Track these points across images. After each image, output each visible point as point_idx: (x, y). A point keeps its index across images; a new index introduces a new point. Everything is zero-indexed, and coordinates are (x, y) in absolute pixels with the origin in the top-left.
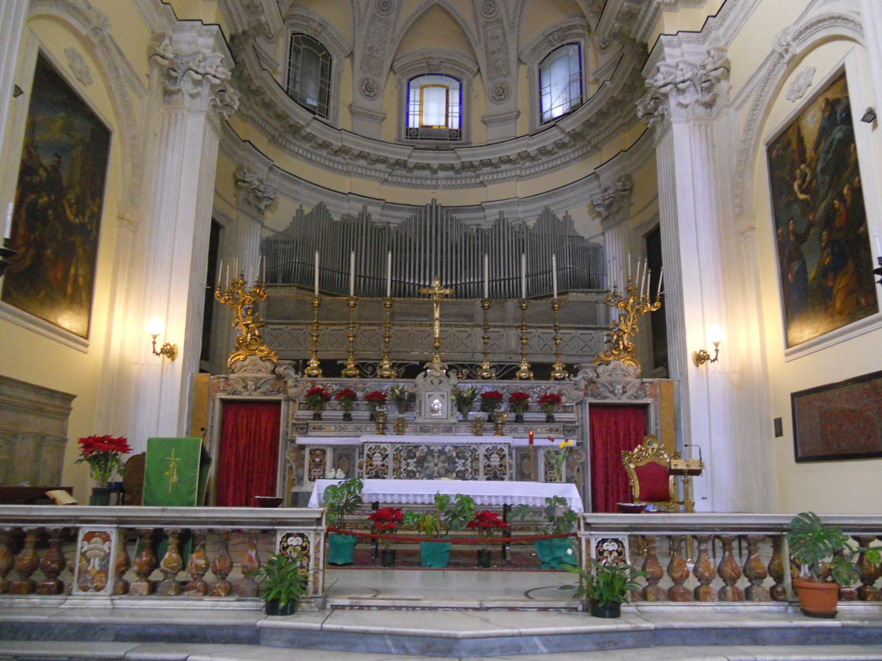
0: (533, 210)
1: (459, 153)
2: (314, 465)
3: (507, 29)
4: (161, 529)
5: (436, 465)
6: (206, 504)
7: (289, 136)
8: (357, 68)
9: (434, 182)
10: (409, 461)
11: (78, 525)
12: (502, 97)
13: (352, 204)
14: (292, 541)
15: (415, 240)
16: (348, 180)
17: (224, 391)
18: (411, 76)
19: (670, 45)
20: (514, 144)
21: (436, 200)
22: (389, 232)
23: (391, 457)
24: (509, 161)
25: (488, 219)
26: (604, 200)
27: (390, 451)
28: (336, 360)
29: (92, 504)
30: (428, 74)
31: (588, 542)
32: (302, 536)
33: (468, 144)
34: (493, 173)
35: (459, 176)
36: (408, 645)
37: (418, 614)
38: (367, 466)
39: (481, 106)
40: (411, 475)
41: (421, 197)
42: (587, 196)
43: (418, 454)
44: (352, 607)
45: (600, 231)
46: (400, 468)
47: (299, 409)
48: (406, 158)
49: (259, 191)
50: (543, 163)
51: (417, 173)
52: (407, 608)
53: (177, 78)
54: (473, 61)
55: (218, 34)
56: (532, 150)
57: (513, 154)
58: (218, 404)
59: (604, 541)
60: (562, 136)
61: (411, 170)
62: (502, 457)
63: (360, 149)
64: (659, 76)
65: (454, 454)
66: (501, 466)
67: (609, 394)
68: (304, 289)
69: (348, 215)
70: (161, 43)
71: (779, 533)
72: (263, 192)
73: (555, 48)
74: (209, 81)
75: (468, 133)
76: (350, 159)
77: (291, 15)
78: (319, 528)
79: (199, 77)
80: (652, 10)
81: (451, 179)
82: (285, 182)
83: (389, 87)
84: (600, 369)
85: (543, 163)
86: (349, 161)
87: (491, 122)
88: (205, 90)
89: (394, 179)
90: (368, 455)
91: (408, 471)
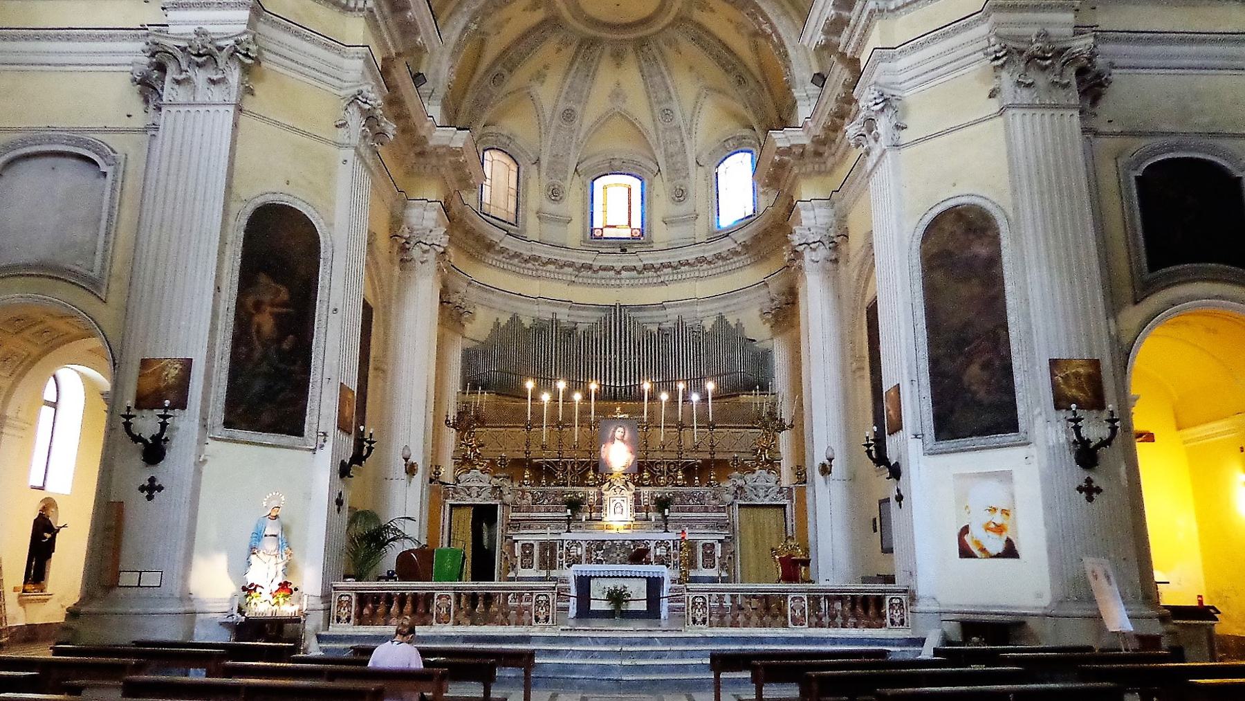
1: (641, 256)
2: (524, 555)
3: (685, 134)
4: (489, 593)
5: (618, 555)
6: (500, 581)
7: (484, 251)
8: (543, 174)
9: (618, 282)
10: (598, 552)
12: (681, 199)
13: (541, 307)
14: (540, 598)
16: (537, 283)
17: (453, 498)
18: (594, 177)
20: (691, 249)
24: (687, 263)
25: (669, 318)
27: (584, 545)
31: (688, 597)
32: (546, 595)
33: (650, 243)
35: (641, 275)
36: (599, 641)
39: (663, 206)
41: (608, 297)
43: (604, 547)
44: (571, 630)
46: (591, 557)
48: (591, 263)
54: (651, 160)
55: (440, 209)
57: (691, 258)
58: (448, 507)
59: (696, 597)
61: (595, 272)
66: (667, 555)
67: (754, 497)
73: (731, 152)
74: (435, 250)
75: (650, 232)
76: (539, 265)
79: (427, 247)
84: (748, 477)
86: (538, 267)
87: (671, 222)
88: (431, 256)
89: (581, 280)
90: (567, 548)
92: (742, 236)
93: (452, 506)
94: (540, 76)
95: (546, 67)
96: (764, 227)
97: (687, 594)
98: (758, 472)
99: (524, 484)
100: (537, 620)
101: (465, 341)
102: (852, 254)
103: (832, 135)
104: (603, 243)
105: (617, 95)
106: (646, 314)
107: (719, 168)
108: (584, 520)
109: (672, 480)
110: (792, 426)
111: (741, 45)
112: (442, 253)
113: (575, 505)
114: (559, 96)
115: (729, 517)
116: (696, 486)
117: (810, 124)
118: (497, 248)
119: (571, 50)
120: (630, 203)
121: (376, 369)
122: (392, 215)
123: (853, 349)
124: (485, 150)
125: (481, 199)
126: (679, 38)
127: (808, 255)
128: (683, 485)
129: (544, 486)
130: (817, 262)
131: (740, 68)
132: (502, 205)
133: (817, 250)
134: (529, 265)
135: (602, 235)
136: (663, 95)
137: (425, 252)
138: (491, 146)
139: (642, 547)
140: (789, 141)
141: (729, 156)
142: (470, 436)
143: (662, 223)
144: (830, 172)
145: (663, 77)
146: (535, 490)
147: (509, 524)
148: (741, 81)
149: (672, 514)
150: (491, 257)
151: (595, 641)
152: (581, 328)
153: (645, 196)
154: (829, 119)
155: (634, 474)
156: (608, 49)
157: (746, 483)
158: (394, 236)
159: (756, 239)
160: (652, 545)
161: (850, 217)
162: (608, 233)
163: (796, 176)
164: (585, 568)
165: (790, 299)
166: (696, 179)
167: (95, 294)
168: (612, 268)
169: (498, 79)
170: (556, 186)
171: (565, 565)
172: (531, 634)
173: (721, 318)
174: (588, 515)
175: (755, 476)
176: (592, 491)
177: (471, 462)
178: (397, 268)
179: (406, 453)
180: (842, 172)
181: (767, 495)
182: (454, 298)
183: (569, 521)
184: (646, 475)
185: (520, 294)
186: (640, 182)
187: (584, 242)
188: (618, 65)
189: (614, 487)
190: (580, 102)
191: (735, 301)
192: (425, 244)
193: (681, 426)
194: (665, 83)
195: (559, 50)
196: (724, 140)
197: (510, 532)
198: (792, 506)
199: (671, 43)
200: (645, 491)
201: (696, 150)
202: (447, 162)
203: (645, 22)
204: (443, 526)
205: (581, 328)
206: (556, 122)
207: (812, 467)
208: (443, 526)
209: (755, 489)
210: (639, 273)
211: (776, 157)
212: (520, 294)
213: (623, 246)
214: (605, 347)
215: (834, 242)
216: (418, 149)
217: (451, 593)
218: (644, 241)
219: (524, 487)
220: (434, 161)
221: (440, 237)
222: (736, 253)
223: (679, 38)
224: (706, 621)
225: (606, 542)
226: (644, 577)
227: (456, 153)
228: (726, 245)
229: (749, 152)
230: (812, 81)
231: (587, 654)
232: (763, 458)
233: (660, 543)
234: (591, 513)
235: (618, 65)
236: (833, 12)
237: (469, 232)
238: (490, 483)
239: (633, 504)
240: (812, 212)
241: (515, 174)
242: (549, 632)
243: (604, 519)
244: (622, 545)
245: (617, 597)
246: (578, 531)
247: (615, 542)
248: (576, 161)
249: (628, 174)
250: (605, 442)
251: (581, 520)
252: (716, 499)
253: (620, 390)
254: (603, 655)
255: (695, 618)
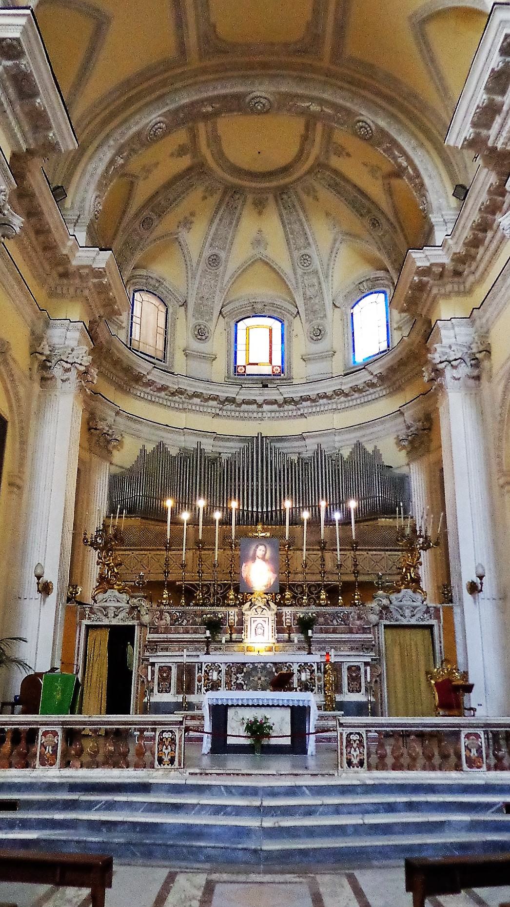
0: (350, 439)
1: (281, 391)
3: (322, 279)
5: (260, 679)
10: (238, 675)
11: (39, 727)
12: (319, 337)
14: (165, 735)
15: (243, 468)
17: (89, 618)
18: (237, 319)
19: (446, 328)
21: (261, 433)
22: (220, 464)
23: (223, 672)
24: (325, 396)
26: (408, 436)
27: (223, 668)
28: (175, 582)
29: (109, 711)
30: (253, 317)
31: (341, 734)
32: (171, 732)
33: (290, 379)
34: (312, 407)
36: (233, 790)
37: (240, 777)
38: (204, 681)
39: (301, 345)
40: (240, 687)
41: (249, 429)
42: (395, 430)
44: (201, 774)
45: (406, 462)
46: (231, 681)
47: (150, 633)
48: (234, 396)
49: (108, 435)
50: (356, 399)
51: (244, 407)
52: (233, 774)
53: (51, 367)
54: (292, 304)
56: (346, 388)
57: (329, 391)
58: (83, 628)
59: (351, 734)
60: (371, 377)
62: (312, 672)
63: (194, 390)
64: (436, 356)
65: (274, 670)
66: (311, 679)
67: (400, 617)
68: (147, 519)
69: (185, 449)
70: (40, 344)
71: (457, 729)
72: (111, 436)
73: (365, 294)
75: (290, 368)
76: (185, 398)
77: (133, 276)
78: (181, 726)
79: (69, 366)
80: (430, 299)
81: (275, 412)
82: (130, 423)
83: (218, 331)
84: (393, 597)
85: (356, 399)
87: (309, 359)
88: (73, 375)
90: (205, 671)
91: (237, 684)
92: (376, 369)
93: (88, 627)
94: (187, 223)
95: (192, 214)
96: (400, 357)
97: (340, 729)
98: (404, 591)
99: (162, 603)
100: (161, 761)
101: (113, 468)
102: (494, 371)
103: (473, 250)
104: (246, 379)
105: (258, 242)
106: (286, 444)
107: (354, 308)
108: (223, 642)
109: (315, 600)
110: (437, 544)
111: (375, 189)
112: (85, 373)
113: (215, 626)
114: (204, 243)
115: (375, 638)
116: (340, 606)
117: (450, 242)
118: (145, 380)
119: (217, 197)
120: (271, 342)
121: (11, 484)
122: (33, 333)
123: (500, 464)
124: (135, 291)
125: (131, 336)
126: (317, 186)
127: (449, 373)
128: (326, 605)
129: (183, 606)
130: (459, 379)
131: (375, 212)
132: (151, 341)
133: (459, 366)
134: (176, 398)
135: (245, 372)
136: (301, 241)
137: (68, 370)
138: (141, 287)
139: (284, 671)
140: (429, 260)
141: (363, 297)
142: (108, 555)
143: (302, 360)
144: (469, 292)
145: (302, 225)
146: (174, 609)
147: (146, 646)
148: (375, 223)
149: (316, 635)
150: (140, 390)
151: (229, 790)
152: (224, 457)
153: (285, 336)
154: (471, 233)
155: (276, 594)
156: (250, 198)
157: (391, 603)
158: (34, 353)
159: (392, 370)
160: (295, 668)
161: (493, 333)
162: (250, 370)
163: (435, 298)
164: (223, 695)
165: (427, 425)
166: (333, 321)
167: (381, 699)
168: (254, 402)
169: (147, 223)
170: (203, 327)
171: (203, 689)
172: (151, 781)
173: (358, 446)
174: (228, 636)
175: (400, 595)
176: (233, 611)
177: (108, 582)
178: (37, 387)
179: (39, 571)
180: (481, 292)
181: (414, 615)
182: (101, 425)
183: (208, 643)
184: (288, 595)
185: (167, 425)
186: (280, 324)
187: (228, 378)
188: (260, 213)
189: (255, 607)
190: (224, 249)
191: (371, 430)
192: (67, 362)
193: (323, 546)
194: (304, 229)
195: (205, 198)
196: (359, 282)
197: (147, 654)
198: (439, 626)
199: (310, 191)
200: (287, 611)
201: (332, 292)
202: (90, 284)
203: (285, 170)
204: (79, 647)
205: (224, 457)
206: (202, 266)
207: (460, 586)
208: (79, 647)
209: (401, 609)
210: (280, 406)
211: (415, 278)
212: (167, 425)
213: (265, 382)
214: (248, 475)
215: (477, 359)
216: (61, 269)
217: (58, 729)
218: (285, 377)
219: (162, 607)
220: (77, 281)
221: (82, 355)
222: (372, 385)
223: (317, 186)
224: (364, 763)
225: (247, 665)
226: (288, 706)
227: (99, 274)
228: (363, 377)
229: (384, 292)
230: (453, 194)
231: (219, 810)
232: (409, 577)
233: (303, 667)
234: (231, 634)
235: (260, 213)
236: (485, 97)
237: (117, 363)
238: (128, 603)
239: (275, 626)
240: (452, 331)
241: (164, 315)
242: (174, 777)
243: (245, 641)
244: (264, 668)
245: (257, 730)
246: (218, 653)
247: (256, 665)
248: (221, 305)
249: (269, 317)
250: (246, 561)
251: (221, 641)
252: (362, 619)
253: (262, 515)
254: (238, 811)
255: (350, 759)
